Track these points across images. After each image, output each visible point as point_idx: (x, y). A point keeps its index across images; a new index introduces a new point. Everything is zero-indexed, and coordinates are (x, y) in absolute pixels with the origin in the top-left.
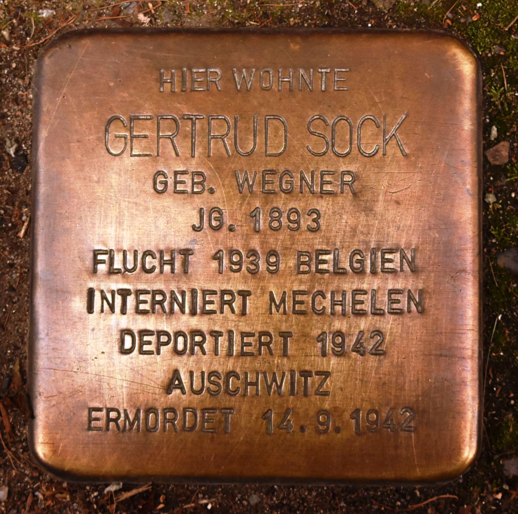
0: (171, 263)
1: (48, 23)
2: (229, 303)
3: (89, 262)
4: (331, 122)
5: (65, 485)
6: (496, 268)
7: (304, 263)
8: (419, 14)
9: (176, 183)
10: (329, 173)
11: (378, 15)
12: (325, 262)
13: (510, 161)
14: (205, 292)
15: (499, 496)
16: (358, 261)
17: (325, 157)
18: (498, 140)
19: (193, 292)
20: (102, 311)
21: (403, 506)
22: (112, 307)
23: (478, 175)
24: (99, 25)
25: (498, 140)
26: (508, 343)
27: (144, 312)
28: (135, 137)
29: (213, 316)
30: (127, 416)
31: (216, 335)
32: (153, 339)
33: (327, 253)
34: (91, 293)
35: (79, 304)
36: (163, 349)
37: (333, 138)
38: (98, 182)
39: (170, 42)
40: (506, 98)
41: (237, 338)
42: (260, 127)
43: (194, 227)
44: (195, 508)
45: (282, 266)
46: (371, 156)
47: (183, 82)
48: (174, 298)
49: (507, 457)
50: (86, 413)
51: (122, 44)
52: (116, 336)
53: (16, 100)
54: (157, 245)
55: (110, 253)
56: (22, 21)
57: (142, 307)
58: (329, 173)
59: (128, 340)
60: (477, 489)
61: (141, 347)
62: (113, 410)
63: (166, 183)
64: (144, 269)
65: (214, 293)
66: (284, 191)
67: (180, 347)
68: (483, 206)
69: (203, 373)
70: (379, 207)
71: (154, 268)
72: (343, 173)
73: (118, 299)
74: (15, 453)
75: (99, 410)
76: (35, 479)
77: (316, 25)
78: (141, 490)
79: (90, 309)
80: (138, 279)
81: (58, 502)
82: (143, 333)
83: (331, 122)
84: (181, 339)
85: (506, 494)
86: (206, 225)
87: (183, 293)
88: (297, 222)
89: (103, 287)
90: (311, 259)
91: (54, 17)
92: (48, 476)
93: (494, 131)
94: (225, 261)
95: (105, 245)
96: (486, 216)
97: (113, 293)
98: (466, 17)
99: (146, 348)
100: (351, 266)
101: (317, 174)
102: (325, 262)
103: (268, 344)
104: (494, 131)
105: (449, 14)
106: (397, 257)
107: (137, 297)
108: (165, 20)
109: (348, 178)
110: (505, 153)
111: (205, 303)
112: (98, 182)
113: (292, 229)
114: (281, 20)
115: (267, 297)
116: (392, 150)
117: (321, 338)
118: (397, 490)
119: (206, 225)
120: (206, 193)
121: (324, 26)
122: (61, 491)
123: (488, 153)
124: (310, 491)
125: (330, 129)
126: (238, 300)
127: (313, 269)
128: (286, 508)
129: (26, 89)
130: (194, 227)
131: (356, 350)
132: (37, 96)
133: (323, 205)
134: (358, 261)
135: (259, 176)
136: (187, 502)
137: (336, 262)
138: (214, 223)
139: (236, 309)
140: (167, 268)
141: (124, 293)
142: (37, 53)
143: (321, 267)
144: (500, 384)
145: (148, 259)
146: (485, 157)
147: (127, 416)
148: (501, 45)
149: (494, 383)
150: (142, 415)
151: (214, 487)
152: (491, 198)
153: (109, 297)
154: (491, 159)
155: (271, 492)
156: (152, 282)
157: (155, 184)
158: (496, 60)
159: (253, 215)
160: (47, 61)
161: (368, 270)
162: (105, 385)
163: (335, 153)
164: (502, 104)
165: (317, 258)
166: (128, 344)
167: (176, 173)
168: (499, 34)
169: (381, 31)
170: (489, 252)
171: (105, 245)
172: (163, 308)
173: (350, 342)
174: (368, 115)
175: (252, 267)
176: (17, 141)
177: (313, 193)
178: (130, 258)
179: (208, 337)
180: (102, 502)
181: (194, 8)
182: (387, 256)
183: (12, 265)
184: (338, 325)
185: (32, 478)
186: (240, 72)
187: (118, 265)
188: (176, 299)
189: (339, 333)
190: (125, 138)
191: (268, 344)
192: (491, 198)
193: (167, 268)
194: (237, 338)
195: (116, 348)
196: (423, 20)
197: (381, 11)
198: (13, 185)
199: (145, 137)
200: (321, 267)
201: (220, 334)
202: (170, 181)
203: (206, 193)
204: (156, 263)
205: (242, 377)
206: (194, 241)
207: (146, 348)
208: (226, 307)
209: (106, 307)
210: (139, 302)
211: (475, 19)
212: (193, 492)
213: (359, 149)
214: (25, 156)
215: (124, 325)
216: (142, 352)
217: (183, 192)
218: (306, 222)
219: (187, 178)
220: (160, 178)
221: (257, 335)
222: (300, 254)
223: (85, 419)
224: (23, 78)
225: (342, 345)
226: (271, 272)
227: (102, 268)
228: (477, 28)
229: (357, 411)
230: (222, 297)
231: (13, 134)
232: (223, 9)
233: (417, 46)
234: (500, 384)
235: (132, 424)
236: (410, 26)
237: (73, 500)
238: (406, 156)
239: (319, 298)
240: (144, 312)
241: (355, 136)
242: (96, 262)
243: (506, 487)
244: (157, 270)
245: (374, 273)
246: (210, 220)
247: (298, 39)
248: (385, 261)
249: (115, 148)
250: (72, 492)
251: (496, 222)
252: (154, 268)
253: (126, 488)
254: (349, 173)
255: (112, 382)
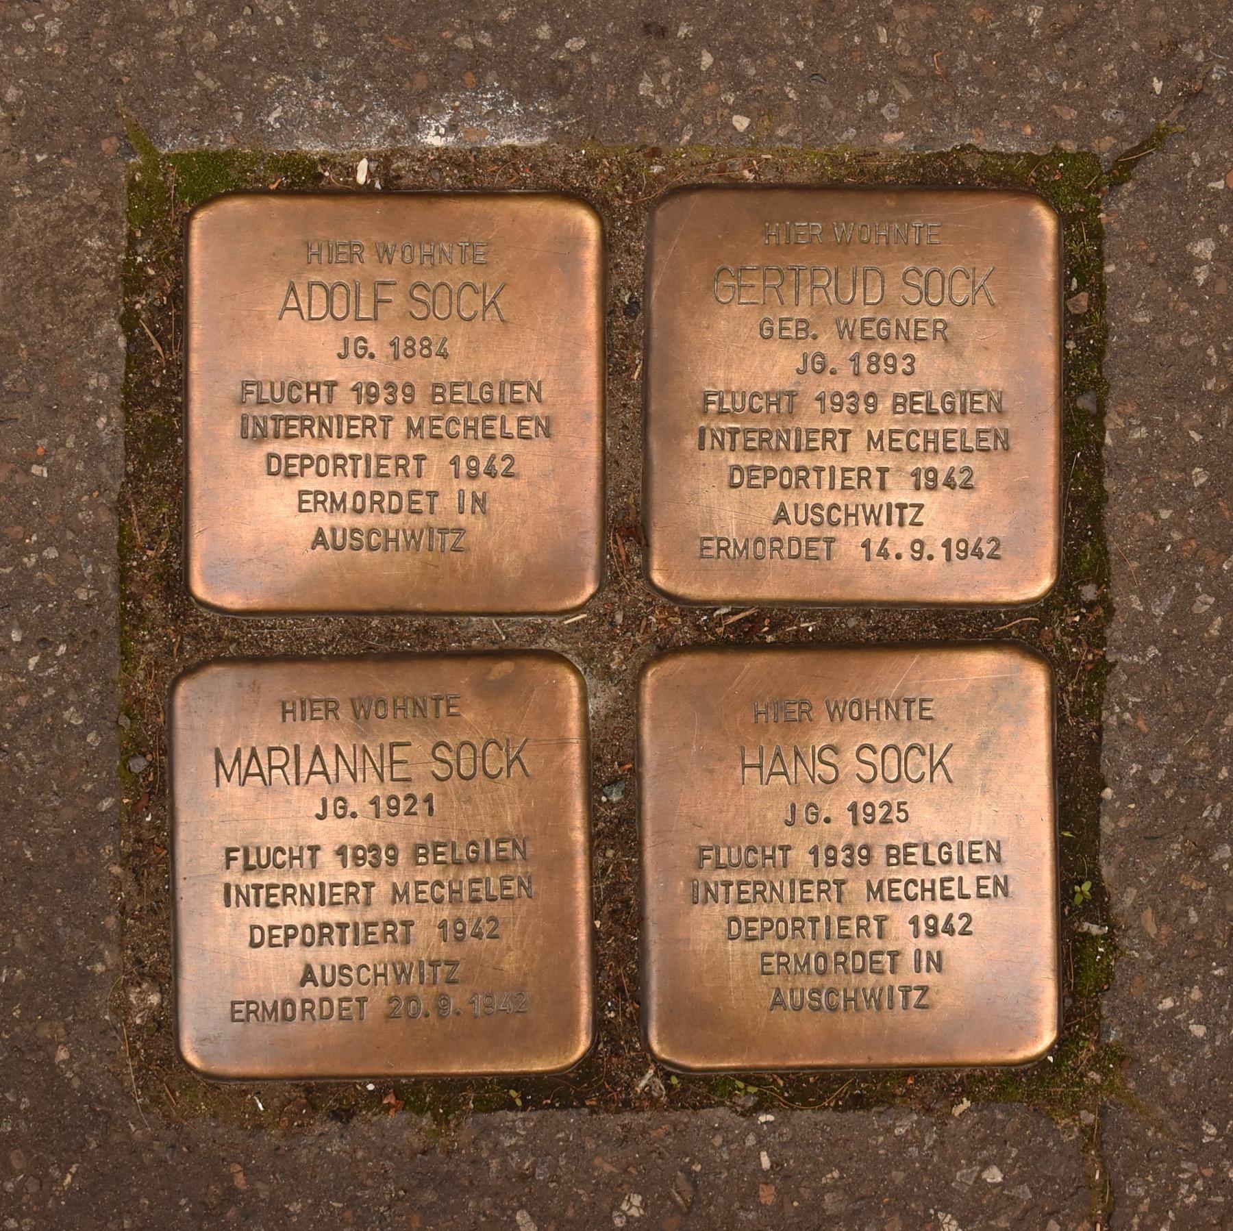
0: (317, 393)
1: (657, 177)
2: (832, 441)
3: (699, 403)
4: (924, 273)
5: (676, 609)
6: (1076, 409)
7: (899, 404)
8: (1005, 173)
9: (781, 329)
10: (922, 321)
11: (968, 173)
12: (918, 403)
13: (1089, 311)
14: (808, 431)
15: (1077, 618)
16: (949, 403)
17: (919, 306)
18: (1078, 291)
19: (798, 431)
20: (713, 448)
21: (989, 628)
22: (722, 444)
23: (1059, 323)
24: (706, 180)
25: (1078, 291)
26: (1086, 479)
27: (752, 449)
28: (742, 286)
29: (816, 453)
30: (736, 546)
31: (819, 470)
32: (760, 474)
33: (920, 394)
34: (702, 431)
35: (691, 442)
36: (770, 483)
37: (926, 288)
38: (707, 328)
39: (775, 197)
40: (1086, 252)
41: (838, 473)
42: (860, 277)
43: (798, 370)
44: (797, 631)
45: (880, 407)
46: (960, 305)
47: (788, 236)
48: (322, 424)
49: (1085, 583)
50: (698, 541)
51: (729, 200)
52: (727, 472)
53: (628, 251)
54: (763, 388)
55: (257, 383)
56: (634, 176)
57: (750, 444)
58: (922, 321)
60: (1057, 612)
61: (749, 481)
62: (723, 539)
63: (772, 330)
64: (752, 410)
66: (881, 337)
67: (786, 482)
68: (1063, 352)
69: (807, 505)
70: (967, 353)
71: (761, 408)
72: (936, 321)
73: (728, 437)
74: (630, 580)
75: (710, 539)
76: (648, 604)
77: (910, 183)
78: (747, 613)
79: (701, 446)
80: (745, 418)
81: (670, 624)
82: (752, 468)
83: (924, 273)
84: (786, 474)
85: (1083, 616)
86: (809, 368)
87: (330, 418)
88: (894, 366)
89: (713, 426)
90: (445, 390)
91: (664, 172)
92: (662, 600)
93: (1075, 282)
94: (828, 401)
95: (714, 386)
96: (1066, 361)
97: (723, 432)
98: (1048, 176)
99: (754, 482)
100: (943, 407)
101: (912, 322)
102: (918, 403)
103: (866, 479)
104: (1075, 282)
105: (1033, 173)
106: (984, 399)
108: (770, 176)
109: (940, 326)
110: (1084, 303)
112: (707, 328)
114: (876, 178)
115: (865, 435)
116: (981, 299)
117: (916, 474)
118: (984, 614)
119: (809, 368)
120: (810, 339)
121: (917, 183)
122: (673, 614)
123: (1068, 303)
124: (904, 614)
125: (923, 279)
126: (380, 425)
127: (448, 398)
128: (880, 630)
129: (639, 240)
130: (798, 370)
131: (947, 484)
132: (649, 247)
133: (917, 351)
134: (949, 403)
135: (859, 323)
136: (791, 624)
137: (929, 403)
138: (818, 367)
140: (313, 398)
142: (651, 207)
143: (455, 398)
144: (1078, 516)
146: (1066, 307)
147: (736, 546)
148: (1081, 202)
149: (1074, 515)
150: (751, 545)
151: (814, 611)
152: (1071, 345)
154: (1071, 309)
155: (867, 615)
156: (760, 421)
157: (761, 330)
158: (1076, 217)
159: (855, 359)
160: (659, 214)
161: (958, 410)
162: (715, 517)
163: (928, 302)
164: (1082, 257)
165: (912, 399)
166: (737, 480)
167: (781, 320)
168: (1077, 192)
169: (970, 189)
170: (1069, 394)
171: (253, 375)
172: (769, 445)
173: (942, 478)
174: (959, 267)
175: (390, 398)
176: (629, 288)
177: (908, 339)
178: (739, 398)
180: (711, 625)
181: (796, 166)
182: (976, 398)
183: (624, 405)
184: (930, 462)
185: (646, 603)
186: (839, 227)
188: (258, 425)
189: (932, 470)
190: (733, 287)
191: (866, 479)
192: (1071, 345)
193: (313, 398)
194: (838, 473)
195: (726, 480)
196: (1009, 178)
197: (970, 170)
198: (627, 331)
199: (752, 286)
200: (455, 398)
201: (823, 469)
202: (776, 327)
203: (810, 339)
204: (763, 403)
205: (843, 508)
206: (798, 383)
207: (754, 482)
208: (828, 444)
209: (716, 444)
211: (1057, 178)
212: (795, 616)
213: (951, 298)
214: (637, 303)
215: (732, 462)
216: (750, 486)
217: (787, 338)
218: (902, 366)
219: (791, 325)
220: (767, 325)
222: (896, 396)
223: (698, 548)
224: (635, 230)
226: (869, 412)
228: (1060, 187)
229: (949, 540)
230: (824, 435)
231: (625, 282)
232: (823, 166)
233: (1004, 203)
234: (1078, 516)
235: (741, 553)
236: (997, 183)
237: (684, 623)
238: (993, 305)
239: (913, 437)
240: (752, 449)
241: (947, 285)
243: (1084, 611)
244: (764, 410)
245: (963, 413)
246: (813, 363)
247: (894, 196)
248: (513, 392)
249: (724, 296)
250: (682, 616)
251: (1075, 367)
252: (761, 408)
253: (733, 613)
254: (941, 321)
255: (723, 513)
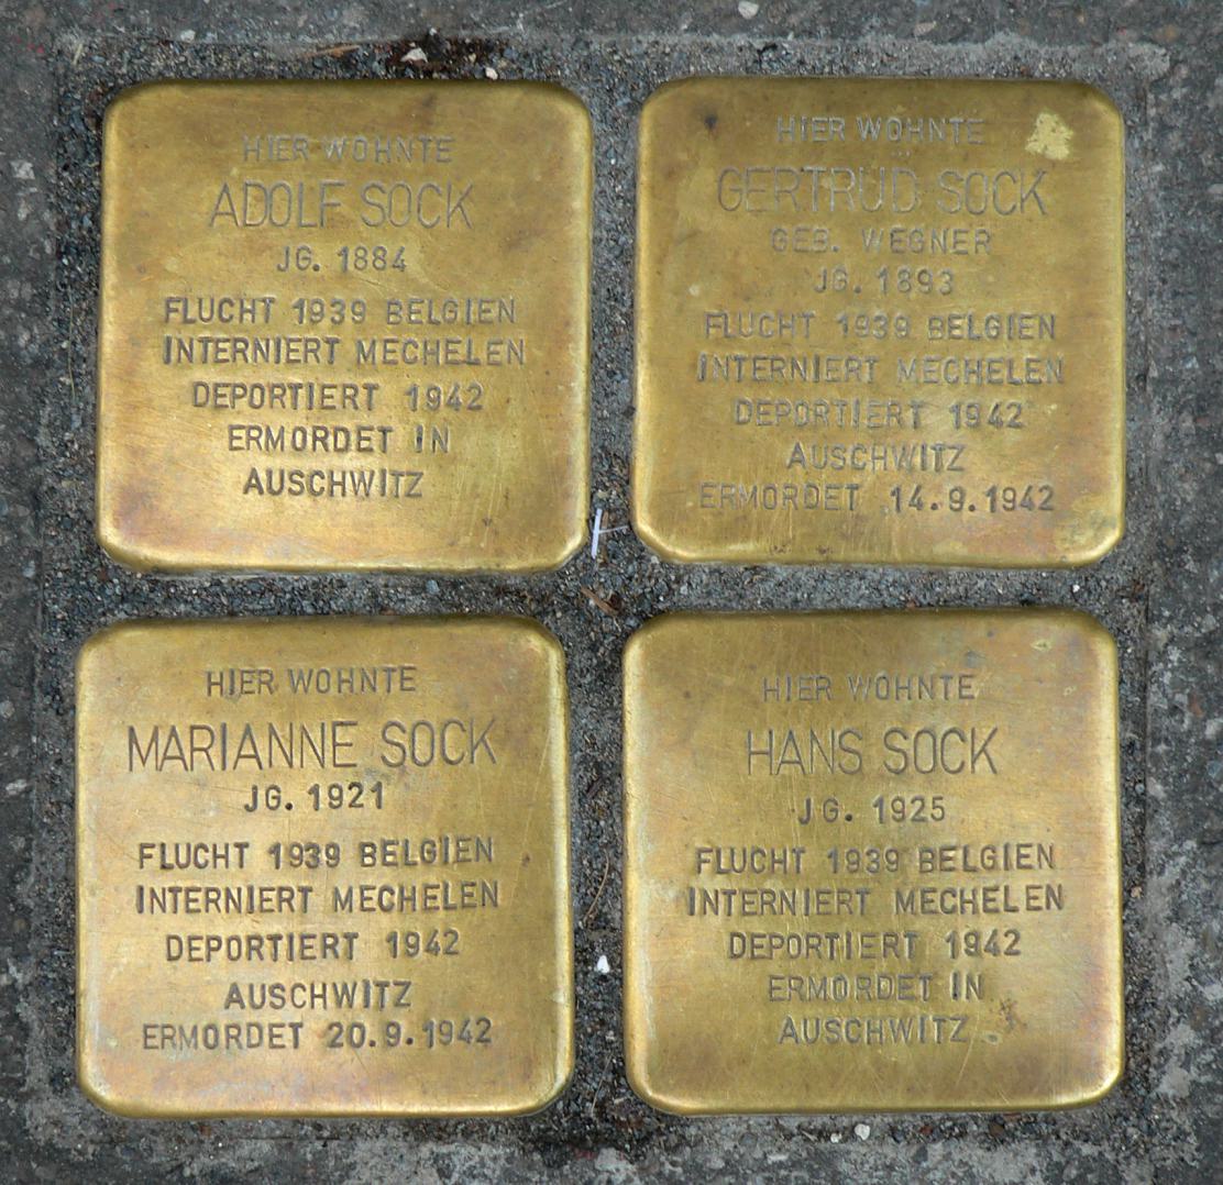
41: (296, 942)
59: (174, 944)
65: (198, 890)
67: (793, 951)
84: (234, 944)
107: (187, 895)
111: (263, 900)
113: (898, 821)
139: (295, 907)
141: (729, 894)
145: (201, 852)
153: (712, 896)
179: (341, 940)
187: (170, 860)
201: (280, 938)
210: (188, 900)
221: (319, 937)
225: (976, 946)
227: (155, 862)
242: (700, 862)
252: (207, 862)
